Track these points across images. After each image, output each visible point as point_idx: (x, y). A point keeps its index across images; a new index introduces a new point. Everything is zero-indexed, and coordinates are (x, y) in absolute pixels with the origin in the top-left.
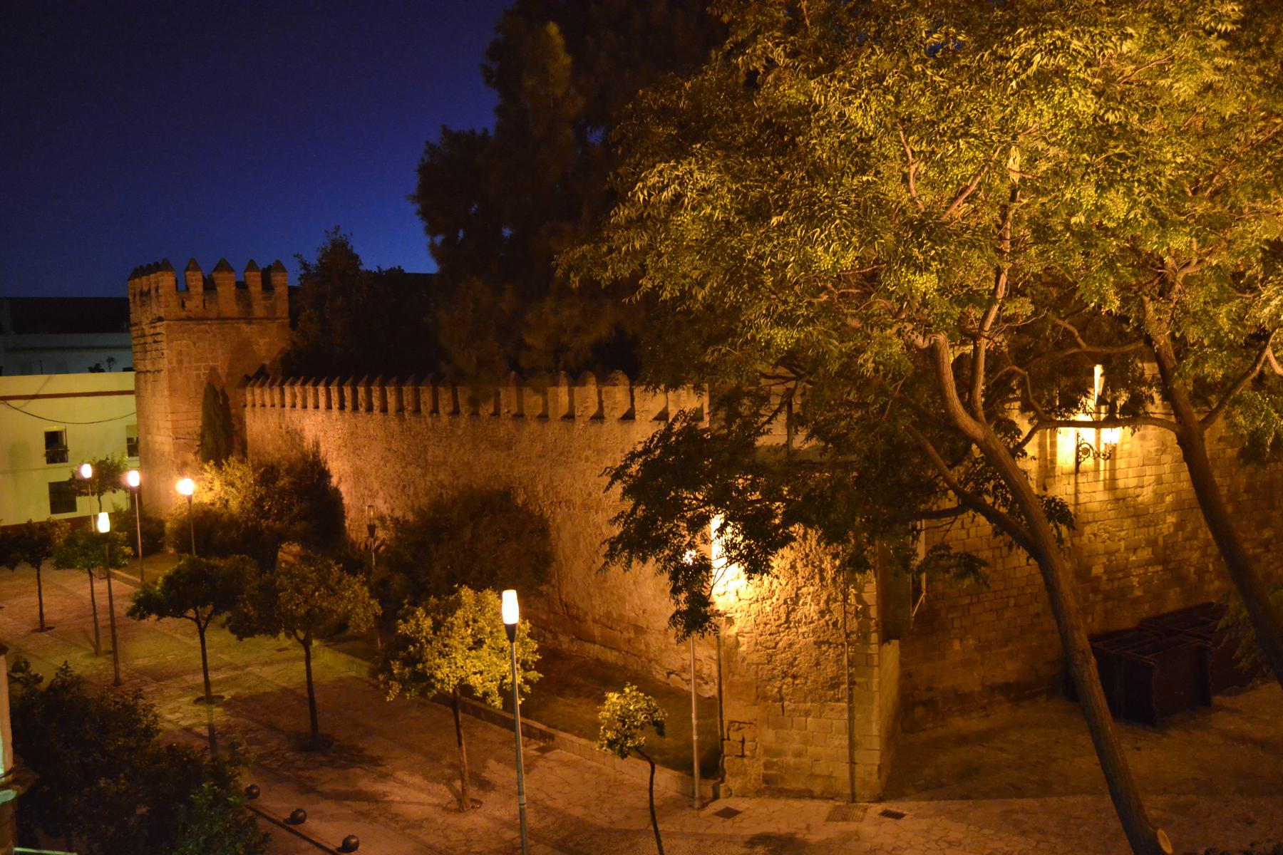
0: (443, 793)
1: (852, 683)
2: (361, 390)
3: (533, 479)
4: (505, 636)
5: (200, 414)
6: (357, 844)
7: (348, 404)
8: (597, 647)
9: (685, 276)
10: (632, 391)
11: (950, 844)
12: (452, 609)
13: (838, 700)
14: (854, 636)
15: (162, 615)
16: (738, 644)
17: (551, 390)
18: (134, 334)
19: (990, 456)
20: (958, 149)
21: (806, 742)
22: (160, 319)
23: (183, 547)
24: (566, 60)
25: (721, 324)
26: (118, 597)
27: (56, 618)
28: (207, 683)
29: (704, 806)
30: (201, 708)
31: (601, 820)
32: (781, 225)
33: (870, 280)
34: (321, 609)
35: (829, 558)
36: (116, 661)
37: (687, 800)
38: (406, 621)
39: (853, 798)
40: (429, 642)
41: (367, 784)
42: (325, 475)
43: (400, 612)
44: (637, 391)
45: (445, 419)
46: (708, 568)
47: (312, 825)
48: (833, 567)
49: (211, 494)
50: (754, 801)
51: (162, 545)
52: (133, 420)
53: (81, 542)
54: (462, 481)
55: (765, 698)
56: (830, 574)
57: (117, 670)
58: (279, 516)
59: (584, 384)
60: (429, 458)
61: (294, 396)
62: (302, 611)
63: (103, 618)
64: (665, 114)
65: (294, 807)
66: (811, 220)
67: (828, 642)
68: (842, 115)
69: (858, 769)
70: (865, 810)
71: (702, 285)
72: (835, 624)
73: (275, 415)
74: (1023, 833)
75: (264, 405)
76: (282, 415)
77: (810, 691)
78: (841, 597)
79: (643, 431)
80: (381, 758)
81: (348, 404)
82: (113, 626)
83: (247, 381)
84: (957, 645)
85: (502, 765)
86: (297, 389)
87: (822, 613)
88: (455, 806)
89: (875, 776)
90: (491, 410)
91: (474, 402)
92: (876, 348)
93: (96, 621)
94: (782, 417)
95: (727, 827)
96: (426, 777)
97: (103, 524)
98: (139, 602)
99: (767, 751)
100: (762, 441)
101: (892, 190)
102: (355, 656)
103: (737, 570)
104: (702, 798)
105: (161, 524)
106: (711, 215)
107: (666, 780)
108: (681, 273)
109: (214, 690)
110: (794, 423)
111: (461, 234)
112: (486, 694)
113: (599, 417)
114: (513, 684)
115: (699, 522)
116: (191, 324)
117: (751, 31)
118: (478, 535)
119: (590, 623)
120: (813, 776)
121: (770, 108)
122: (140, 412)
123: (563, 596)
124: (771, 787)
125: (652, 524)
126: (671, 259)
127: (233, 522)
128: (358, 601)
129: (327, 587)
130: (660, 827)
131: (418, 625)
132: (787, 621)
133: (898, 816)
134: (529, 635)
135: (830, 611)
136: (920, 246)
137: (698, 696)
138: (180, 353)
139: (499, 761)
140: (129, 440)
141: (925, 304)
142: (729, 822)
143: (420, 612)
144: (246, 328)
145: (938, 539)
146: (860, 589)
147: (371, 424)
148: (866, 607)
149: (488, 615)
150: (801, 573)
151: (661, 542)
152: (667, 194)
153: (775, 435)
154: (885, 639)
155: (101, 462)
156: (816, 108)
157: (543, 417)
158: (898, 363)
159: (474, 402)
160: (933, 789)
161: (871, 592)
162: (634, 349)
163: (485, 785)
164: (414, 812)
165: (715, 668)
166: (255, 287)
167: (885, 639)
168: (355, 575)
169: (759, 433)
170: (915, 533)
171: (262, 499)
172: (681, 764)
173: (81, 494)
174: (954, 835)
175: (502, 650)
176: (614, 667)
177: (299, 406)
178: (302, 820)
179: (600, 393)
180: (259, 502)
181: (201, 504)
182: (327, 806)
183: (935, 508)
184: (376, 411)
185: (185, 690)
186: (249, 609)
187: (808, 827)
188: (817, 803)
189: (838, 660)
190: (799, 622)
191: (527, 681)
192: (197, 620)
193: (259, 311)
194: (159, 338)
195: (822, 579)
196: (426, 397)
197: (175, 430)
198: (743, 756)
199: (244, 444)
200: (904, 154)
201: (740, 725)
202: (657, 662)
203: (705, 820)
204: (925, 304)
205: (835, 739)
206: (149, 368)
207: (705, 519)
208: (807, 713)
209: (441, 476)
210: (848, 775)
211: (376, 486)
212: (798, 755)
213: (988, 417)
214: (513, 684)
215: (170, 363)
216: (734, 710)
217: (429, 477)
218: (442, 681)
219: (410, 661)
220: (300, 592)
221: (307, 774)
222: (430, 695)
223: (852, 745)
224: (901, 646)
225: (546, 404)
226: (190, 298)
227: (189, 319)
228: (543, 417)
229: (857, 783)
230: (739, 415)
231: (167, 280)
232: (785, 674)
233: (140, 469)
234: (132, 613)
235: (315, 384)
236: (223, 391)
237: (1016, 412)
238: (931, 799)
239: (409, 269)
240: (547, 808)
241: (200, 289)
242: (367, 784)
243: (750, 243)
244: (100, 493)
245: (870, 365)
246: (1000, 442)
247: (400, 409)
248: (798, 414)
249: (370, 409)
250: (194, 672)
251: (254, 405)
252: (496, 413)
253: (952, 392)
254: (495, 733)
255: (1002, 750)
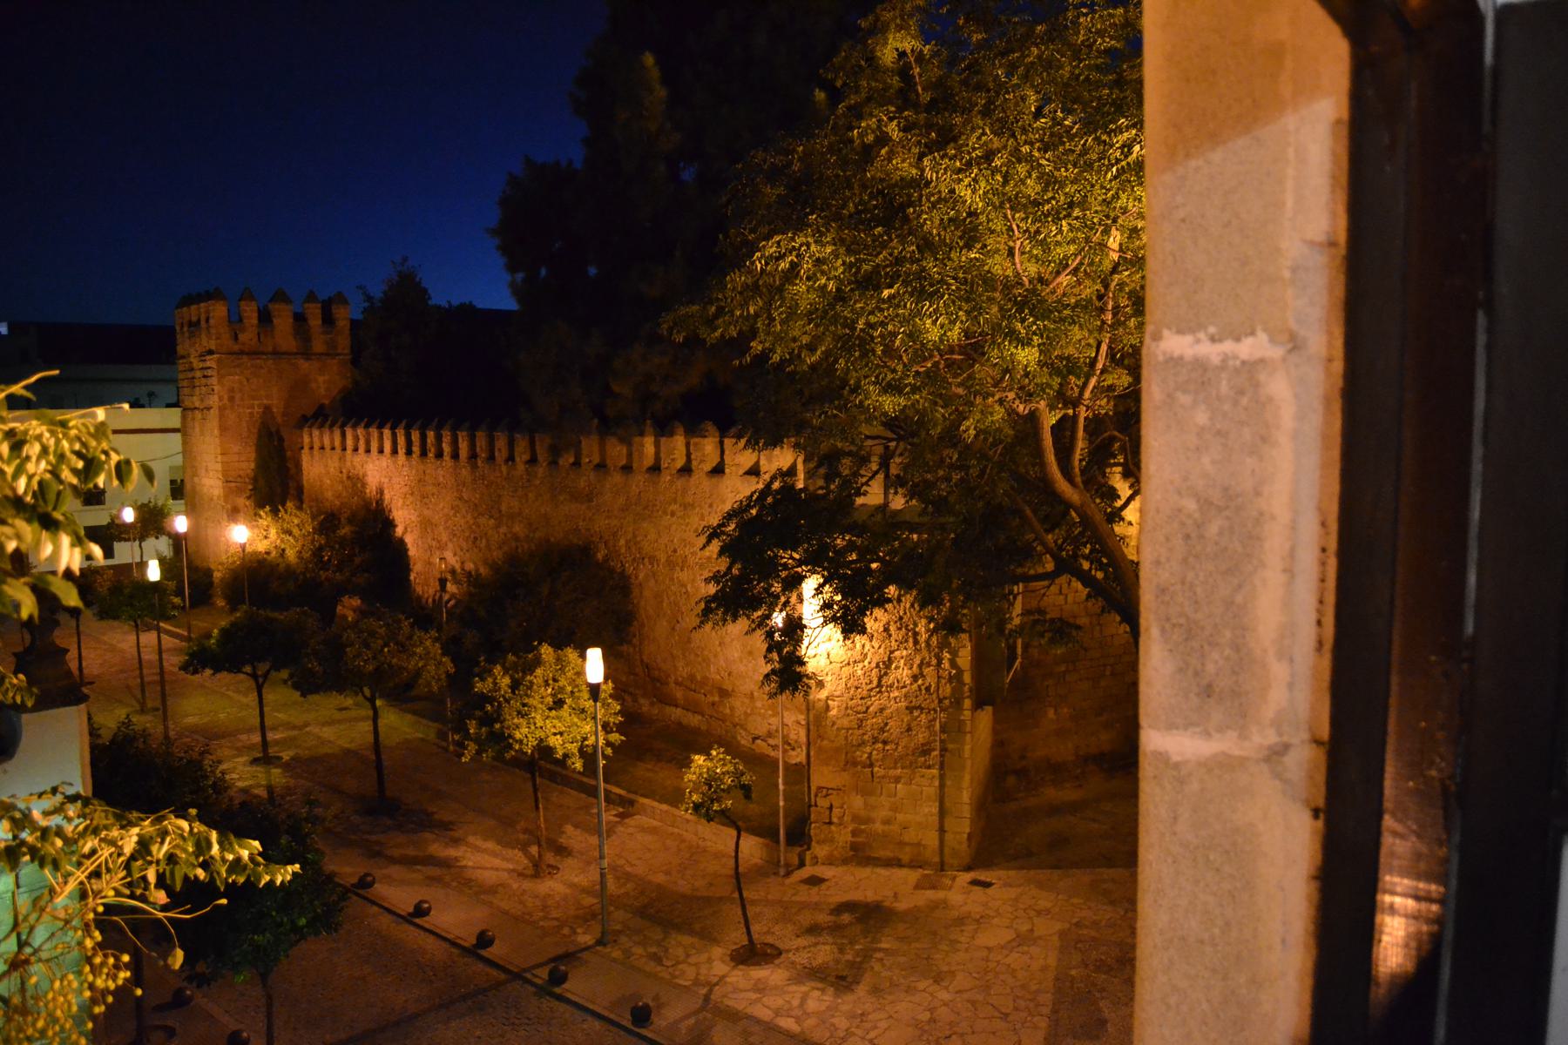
0: (519, 859)
1: (944, 750)
2: (431, 435)
3: (615, 534)
4: (586, 695)
5: (253, 456)
6: (429, 909)
7: (416, 449)
8: (679, 710)
9: (794, 340)
10: (722, 443)
11: (1039, 913)
12: (530, 668)
13: (929, 767)
14: (947, 702)
15: (217, 670)
16: (828, 708)
17: (637, 439)
18: (181, 368)
19: (1086, 521)
20: (1060, 231)
21: (895, 809)
22: (211, 352)
23: (234, 600)
24: (661, 92)
25: (828, 388)
26: (169, 650)
27: (96, 672)
28: (265, 744)
29: (788, 874)
30: (259, 770)
31: (683, 886)
32: (892, 297)
33: (973, 349)
34: (390, 666)
35: (924, 621)
36: (165, 719)
37: (772, 867)
38: (483, 679)
39: (942, 867)
40: (507, 701)
41: (438, 849)
42: (390, 524)
43: (476, 670)
44: (728, 442)
45: (521, 467)
46: (803, 627)
47: (380, 889)
48: (928, 630)
49: (266, 542)
50: (840, 869)
51: (210, 597)
52: (178, 460)
53: (127, 591)
54: (538, 535)
55: (855, 764)
56: (923, 637)
57: (166, 728)
58: (339, 568)
59: (672, 434)
60: (504, 508)
61: (357, 439)
62: (371, 668)
63: (151, 675)
64: (774, 175)
65: (362, 871)
66: (921, 295)
67: (920, 708)
68: (952, 191)
69: (948, 837)
70: (954, 879)
71: (812, 348)
72: (928, 689)
73: (336, 458)
74: (1112, 903)
75: (322, 448)
76: (342, 459)
77: (901, 758)
78: (934, 662)
79: (736, 490)
80: (451, 823)
81: (416, 449)
82: (162, 682)
83: (305, 421)
84: (1051, 713)
85: (578, 832)
86: (360, 431)
87: (915, 678)
88: (530, 872)
89: (965, 846)
90: (572, 460)
91: (555, 452)
92: (978, 416)
93: (142, 677)
94: (881, 476)
95: (814, 894)
96: (499, 842)
97: (154, 573)
98: (192, 655)
99: (856, 818)
100: (860, 501)
101: (998, 266)
102: (424, 717)
103: (834, 632)
104: (787, 865)
105: (208, 573)
106: (825, 286)
107: (752, 848)
108: (789, 336)
109: (272, 751)
110: (891, 484)
111: (543, 272)
112: (566, 756)
113: (686, 470)
114: (595, 747)
115: (795, 582)
116: (245, 358)
117: (863, 95)
118: (557, 591)
119: (672, 685)
120: (902, 844)
121: (882, 180)
122: (187, 451)
123: (645, 658)
124: (859, 855)
125: (749, 584)
126: (782, 322)
127: (290, 572)
128: (430, 659)
129: (397, 644)
130: (745, 894)
131: (495, 684)
132: (879, 685)
133: (987, 885)
134: (611, 696)
135: (923, 676)
136: (1023, 321)
137: (785, 763)
138: (232, 390)
139: (576, 826)
140: (173, 482)
141: (1027, 375)
142: (816, 889)
143: (497, 670)
144: (304, 365)
145: (1034, 604)
146: (954, 653)
147: (442, 471)
148: (960, 672)
149: (569, 674)
150: (894, 636)
151: (754, 603)
152: (783, 265)
153: (874, 495)
154: (978, 705)
155: (143, 505)
156: (928, 184)
157: (627, 469)
158: (999, 430)
159: (555, 452)
160: (1022, 858)
161: (965, 658)
162: (735, 399)
163: (562, 851)
164: (489, 877)
165: (803, 733)
166: (315, 322)
167: (978, 705)
168: (427, 631)
169: (859, 494)
170: (1008, 599)
171: (321, 548)
172: (767, 831)
173: (120, 540)
174: (1043, 904)
175: (583, 711)
176: (696, 731)
177: (361, 450)
178: (371, 885)
179: (688, 445)
180: (318, 552)
181: (255, 553)
182: (395, 871)
183: (1032, 572)
184: (447, 457)
185: (240, 751)
186: (314, 665)
187: (896, 896)
188: (904, 872)
189: (930, 726)
190: (891, 686)
191: (608, 744)
192: (254, 676)
193: (318, 345)
194: (209, 372)
195: (916, 642)
196: (501, 443)
197: (225, 473)
198: (830, 823)
199: (300, 489)
200: (1010, 229)
201: (825, 791)
202: (742, 726)
203: (791, 888)
204: (1027, 375)
205: (923, 807)
206: (197, 404)
207: (800, 579)
208: (897, 780)
209: (517, 528)
210: (937, 843)
211: (444, 537)
212: (887, 822)
213: (1085, 483)
214: (595, 747)
215: (221, 399)
216: (822, 776)
217: (503, 530)
218: (521, 742)
219: (487, 721)
220: (368, 646)
221: (374, 838)
222: (508, 756)
223: (942, 812)
224: (994, 714)
225: (630, 455)
226: (243, 330)
227: (242, 353)
228: (627, 469)
229: (947, 850)
230: (839, 475)
231: (219, 310)
232: (875, 740)
233: (187, 514)
234: (184, 667)
235: (380, 427)
236: (278, 432)
237: (1118, 476)
238: (1022, 868)
239: (482, 303)
240: (628, 874)
241: (255, 321)
242: (438, 849)
243: (862, 313)
244: (142, 539)
245: (972, 432)
246: (1096, 508)
247: (473, 456)
248: (898, 476)
249: (439, 455)
250: (250, 731)
251: (312, 448)
252: (577, 464)
253: (1051, 457)
254: (572, 798)
255: (1094, 820)
